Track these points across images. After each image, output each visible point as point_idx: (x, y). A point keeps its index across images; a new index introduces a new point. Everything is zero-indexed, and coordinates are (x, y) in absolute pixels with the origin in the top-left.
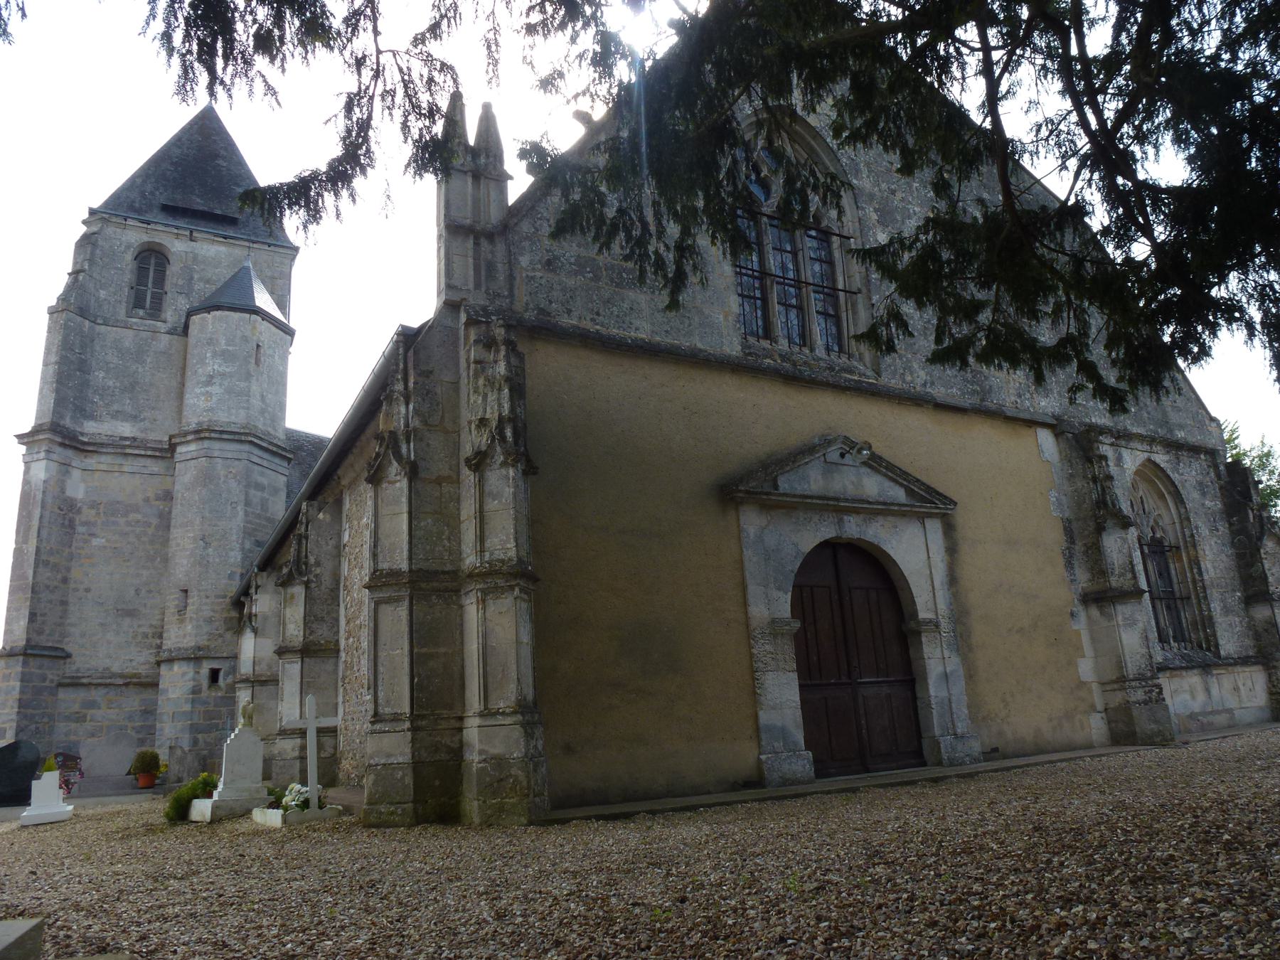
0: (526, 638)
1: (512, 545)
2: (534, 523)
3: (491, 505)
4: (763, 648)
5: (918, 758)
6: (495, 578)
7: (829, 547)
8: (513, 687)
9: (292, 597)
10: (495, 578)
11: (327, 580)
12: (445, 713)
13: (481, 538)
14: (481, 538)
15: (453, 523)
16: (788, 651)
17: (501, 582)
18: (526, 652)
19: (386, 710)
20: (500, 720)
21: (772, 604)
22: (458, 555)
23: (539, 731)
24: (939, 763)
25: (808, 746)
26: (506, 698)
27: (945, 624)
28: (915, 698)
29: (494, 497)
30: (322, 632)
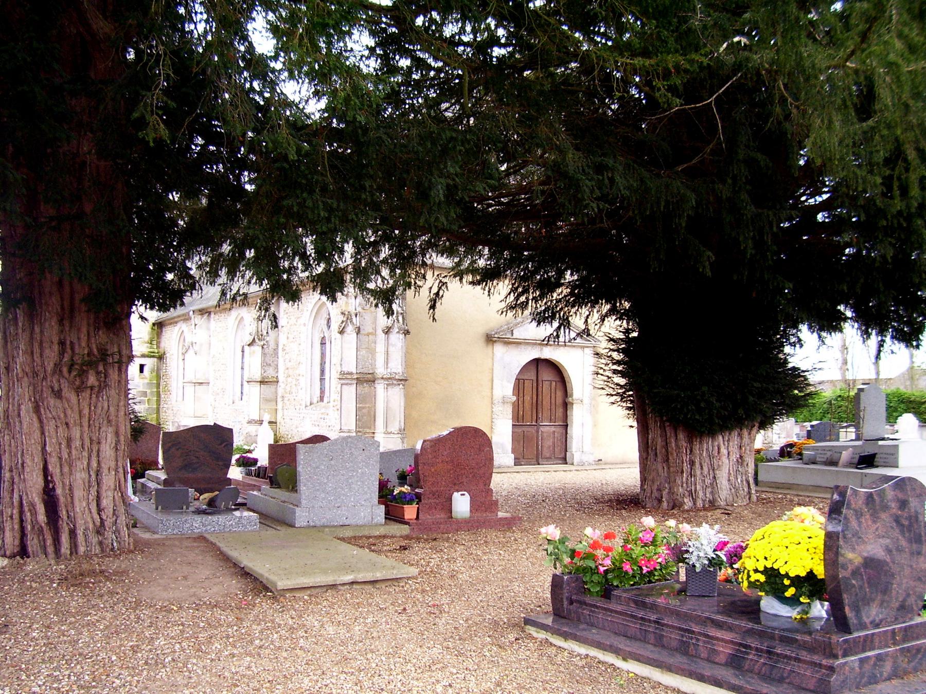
0: (402, 404)
1: (400, 367)
2: (408, 362)
3: (391, 349)
4: (498, 408)
5: (564, 461)
6: (391, 381)
7: (537, 362)
8: (397, 423)
9: (254, 352)
10: (391, 381)
11: (272, 345)
12: (368, 431)
13: (387, 362)
14: (387, 362)
15: (373, 352)
16: (508, 411)
17: (395, 382)
18: (402, 408)
19: (344, 428)
20: (392, 435)
21: (505, 388)
22: (373, 365)
23: (406, 440)
24: (573, 464)
25: (513, 451)
26: (395, 427)
27: (586, 401)
28: (566, 433)
29: (393, 346)
30: (270, 372)
